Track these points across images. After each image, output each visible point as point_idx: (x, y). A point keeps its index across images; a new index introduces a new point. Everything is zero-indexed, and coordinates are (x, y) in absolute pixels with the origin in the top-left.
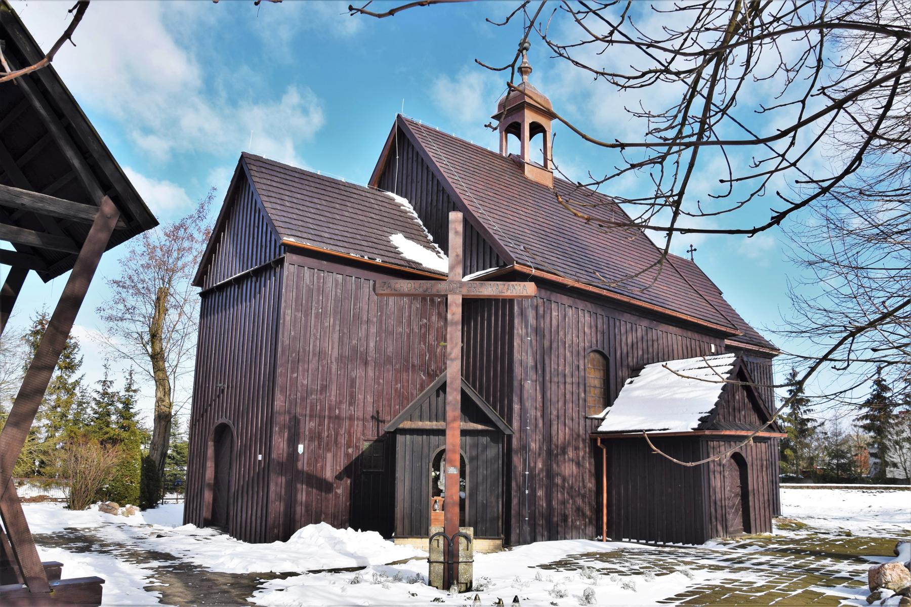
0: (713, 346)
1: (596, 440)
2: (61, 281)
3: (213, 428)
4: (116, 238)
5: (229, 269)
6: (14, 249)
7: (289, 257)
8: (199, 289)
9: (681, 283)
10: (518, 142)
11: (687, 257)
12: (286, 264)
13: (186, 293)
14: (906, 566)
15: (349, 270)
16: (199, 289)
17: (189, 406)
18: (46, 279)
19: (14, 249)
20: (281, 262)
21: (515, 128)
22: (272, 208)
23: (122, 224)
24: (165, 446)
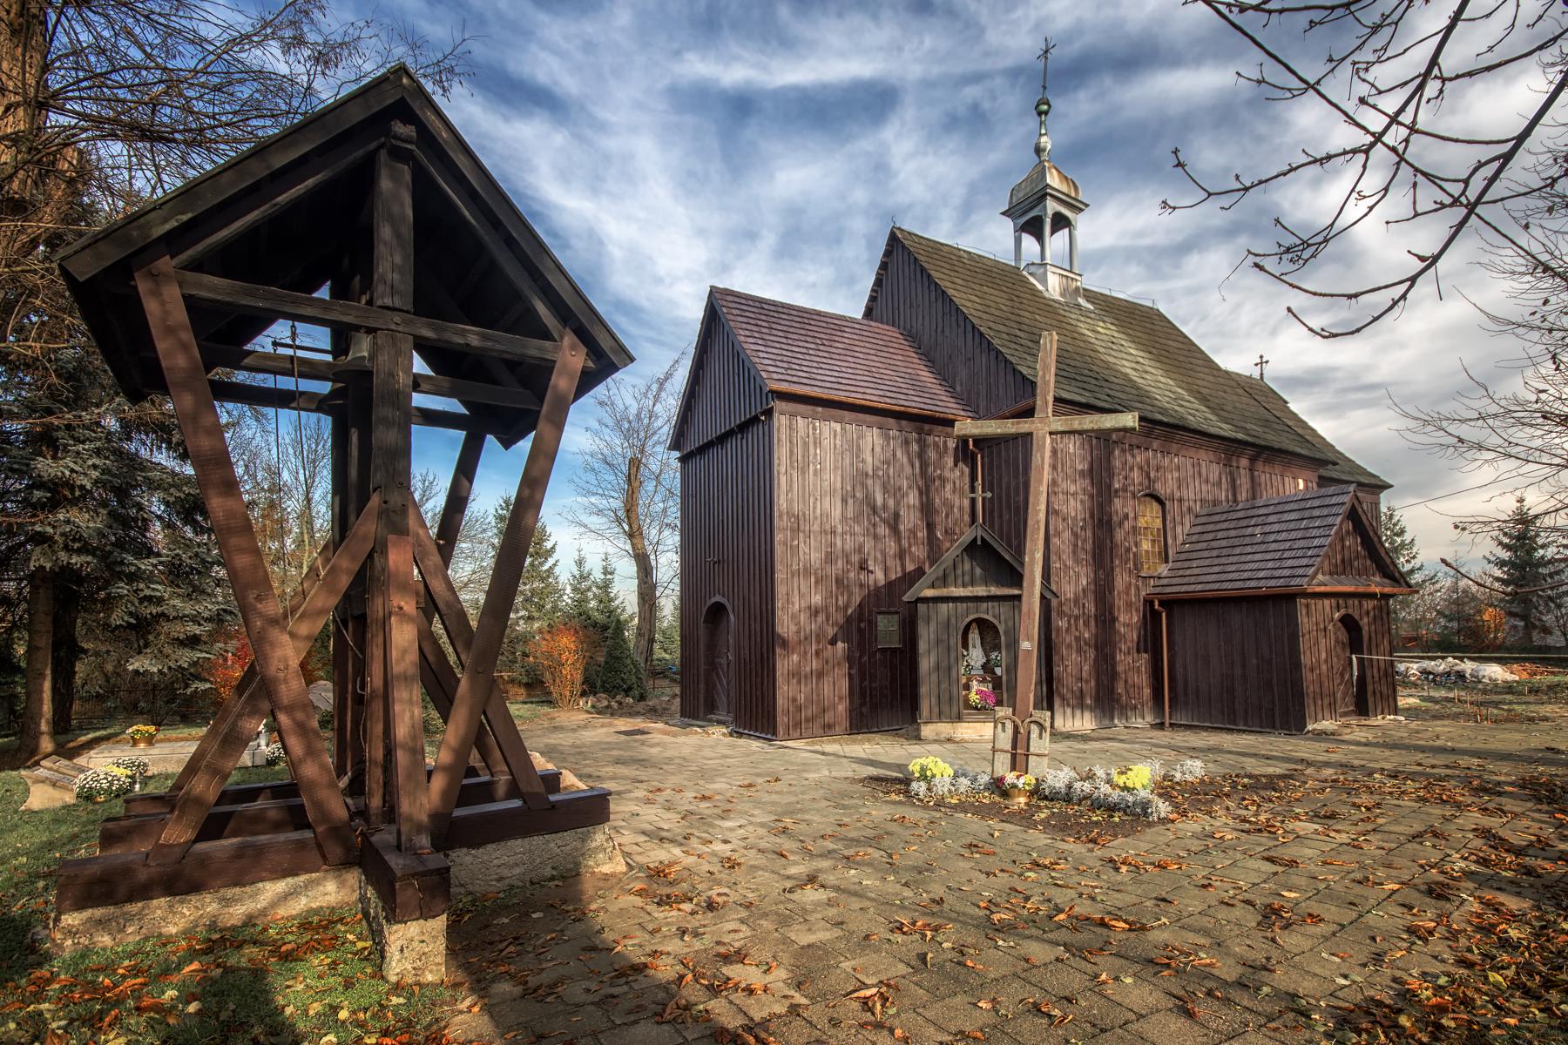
0: (1301, 482)
1: (1152, 603)
2: (525, 445)
3: (704, 610)
4: (587, 381)
5: (706, 428)
6: (464, 411)
7: (779, 405)
8: (677, 454)
9: (486, 163)
10: (1037, 247)
11: (1256, 374)
12: (776, 415)
13: (664, 463)
14: (1031, 434)
15: (847, 415)
16: (677, 454)
17: (676, 585)
18: (507, 443)
19: (464, 411)
20: (769, 413)
21: (1034, 228)
22: (750, 345)
23: (591, 364)
24: (652, 631)
